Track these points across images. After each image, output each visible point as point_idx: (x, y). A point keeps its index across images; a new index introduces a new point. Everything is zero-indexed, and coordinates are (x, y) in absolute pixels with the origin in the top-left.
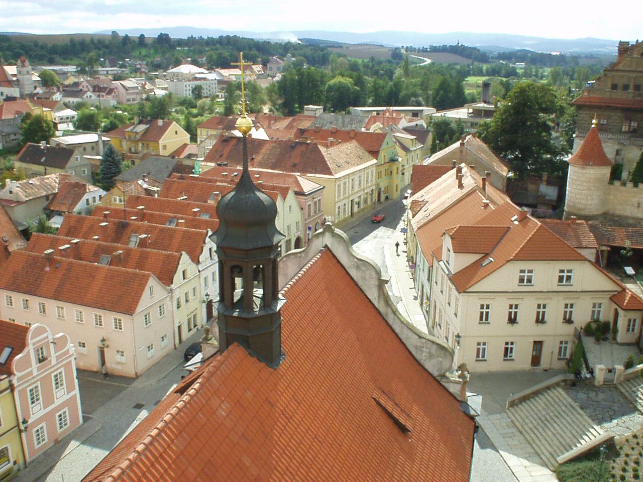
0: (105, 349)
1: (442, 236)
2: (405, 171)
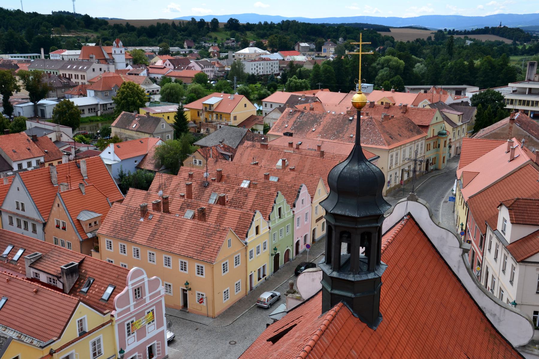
0: (188, 292)
1: (498, 207)
2: (452, 144)
